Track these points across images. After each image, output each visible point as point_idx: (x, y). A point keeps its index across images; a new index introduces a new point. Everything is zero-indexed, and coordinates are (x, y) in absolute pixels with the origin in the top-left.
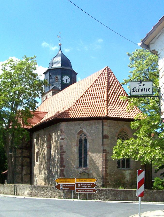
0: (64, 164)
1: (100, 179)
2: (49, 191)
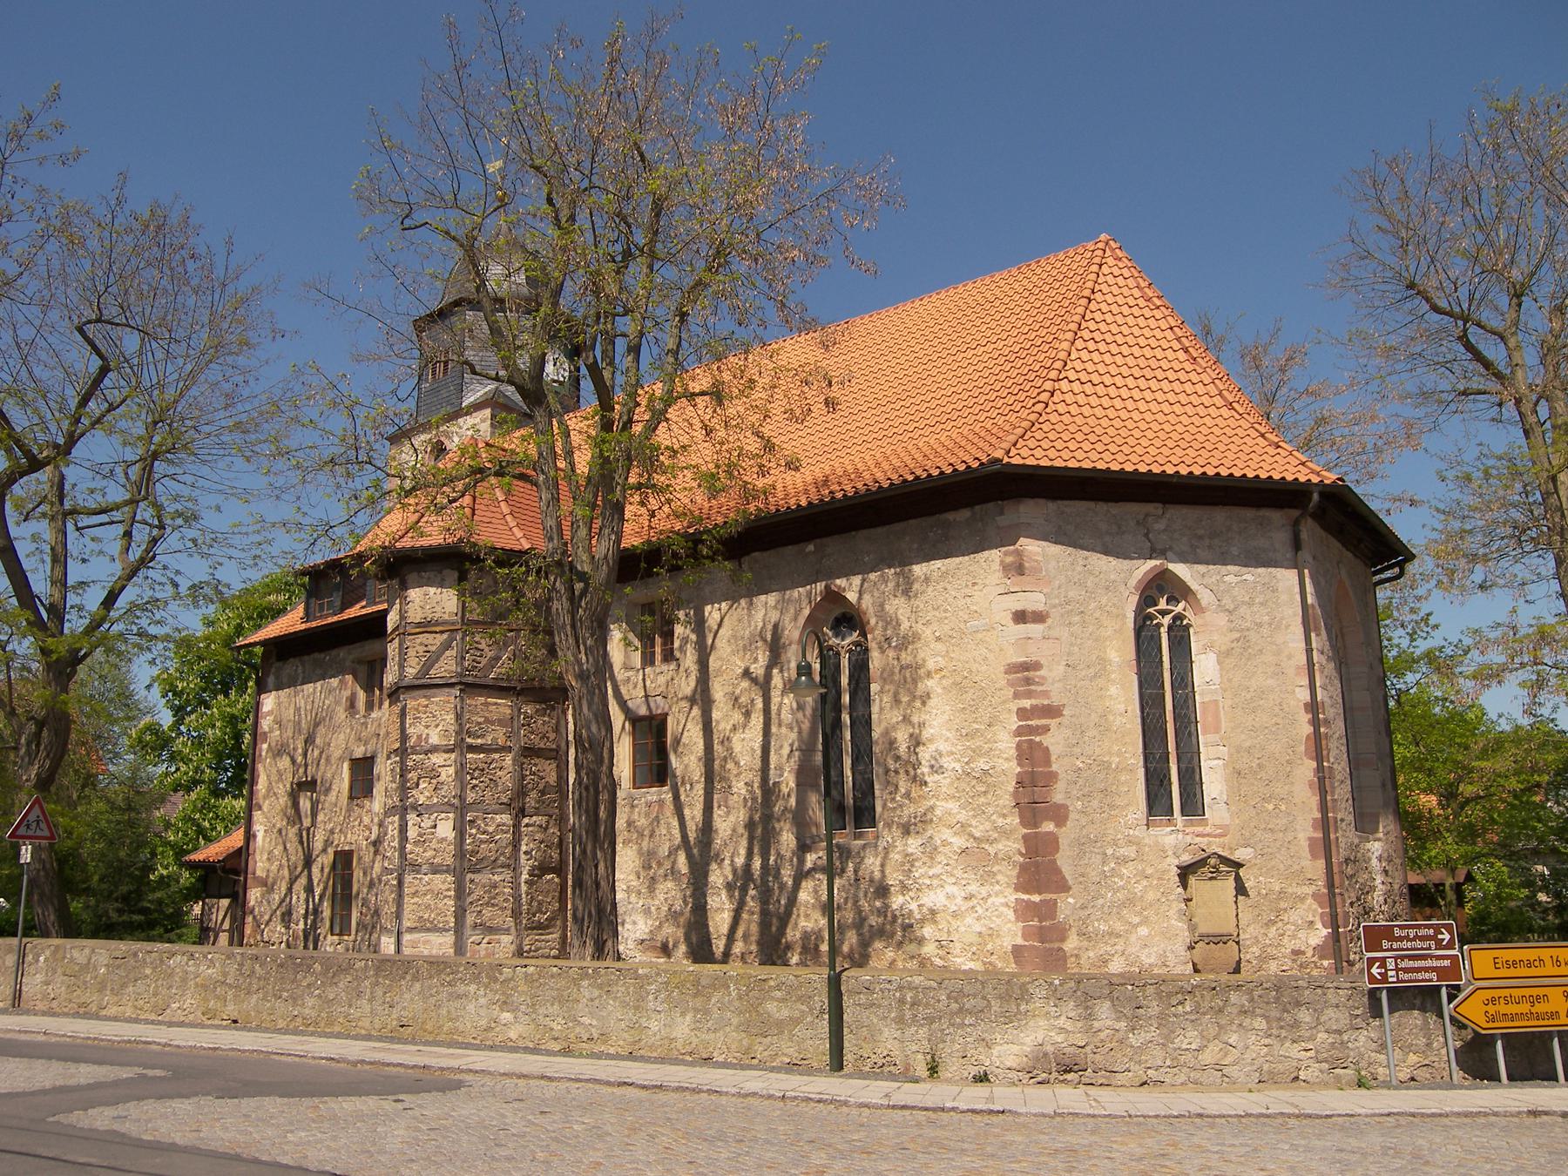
0: (1058, 797)
1: (1310, 901)
2: (1247, 1022)
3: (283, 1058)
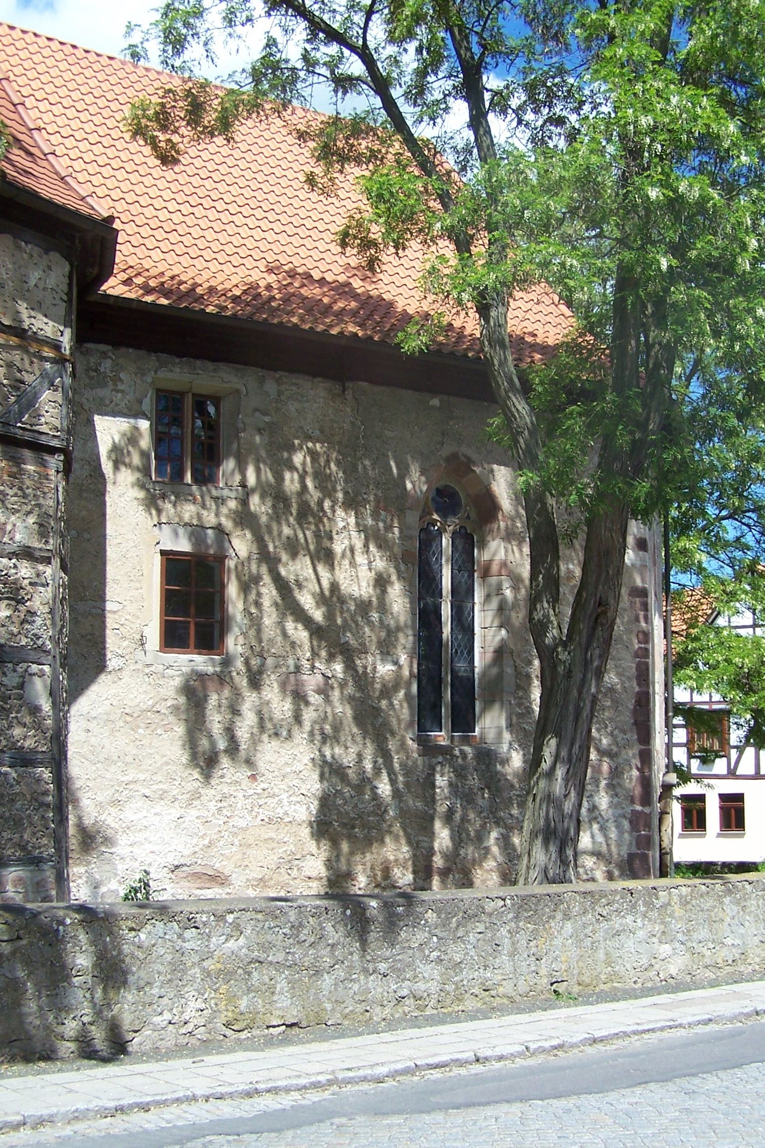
3: (138, 1121)
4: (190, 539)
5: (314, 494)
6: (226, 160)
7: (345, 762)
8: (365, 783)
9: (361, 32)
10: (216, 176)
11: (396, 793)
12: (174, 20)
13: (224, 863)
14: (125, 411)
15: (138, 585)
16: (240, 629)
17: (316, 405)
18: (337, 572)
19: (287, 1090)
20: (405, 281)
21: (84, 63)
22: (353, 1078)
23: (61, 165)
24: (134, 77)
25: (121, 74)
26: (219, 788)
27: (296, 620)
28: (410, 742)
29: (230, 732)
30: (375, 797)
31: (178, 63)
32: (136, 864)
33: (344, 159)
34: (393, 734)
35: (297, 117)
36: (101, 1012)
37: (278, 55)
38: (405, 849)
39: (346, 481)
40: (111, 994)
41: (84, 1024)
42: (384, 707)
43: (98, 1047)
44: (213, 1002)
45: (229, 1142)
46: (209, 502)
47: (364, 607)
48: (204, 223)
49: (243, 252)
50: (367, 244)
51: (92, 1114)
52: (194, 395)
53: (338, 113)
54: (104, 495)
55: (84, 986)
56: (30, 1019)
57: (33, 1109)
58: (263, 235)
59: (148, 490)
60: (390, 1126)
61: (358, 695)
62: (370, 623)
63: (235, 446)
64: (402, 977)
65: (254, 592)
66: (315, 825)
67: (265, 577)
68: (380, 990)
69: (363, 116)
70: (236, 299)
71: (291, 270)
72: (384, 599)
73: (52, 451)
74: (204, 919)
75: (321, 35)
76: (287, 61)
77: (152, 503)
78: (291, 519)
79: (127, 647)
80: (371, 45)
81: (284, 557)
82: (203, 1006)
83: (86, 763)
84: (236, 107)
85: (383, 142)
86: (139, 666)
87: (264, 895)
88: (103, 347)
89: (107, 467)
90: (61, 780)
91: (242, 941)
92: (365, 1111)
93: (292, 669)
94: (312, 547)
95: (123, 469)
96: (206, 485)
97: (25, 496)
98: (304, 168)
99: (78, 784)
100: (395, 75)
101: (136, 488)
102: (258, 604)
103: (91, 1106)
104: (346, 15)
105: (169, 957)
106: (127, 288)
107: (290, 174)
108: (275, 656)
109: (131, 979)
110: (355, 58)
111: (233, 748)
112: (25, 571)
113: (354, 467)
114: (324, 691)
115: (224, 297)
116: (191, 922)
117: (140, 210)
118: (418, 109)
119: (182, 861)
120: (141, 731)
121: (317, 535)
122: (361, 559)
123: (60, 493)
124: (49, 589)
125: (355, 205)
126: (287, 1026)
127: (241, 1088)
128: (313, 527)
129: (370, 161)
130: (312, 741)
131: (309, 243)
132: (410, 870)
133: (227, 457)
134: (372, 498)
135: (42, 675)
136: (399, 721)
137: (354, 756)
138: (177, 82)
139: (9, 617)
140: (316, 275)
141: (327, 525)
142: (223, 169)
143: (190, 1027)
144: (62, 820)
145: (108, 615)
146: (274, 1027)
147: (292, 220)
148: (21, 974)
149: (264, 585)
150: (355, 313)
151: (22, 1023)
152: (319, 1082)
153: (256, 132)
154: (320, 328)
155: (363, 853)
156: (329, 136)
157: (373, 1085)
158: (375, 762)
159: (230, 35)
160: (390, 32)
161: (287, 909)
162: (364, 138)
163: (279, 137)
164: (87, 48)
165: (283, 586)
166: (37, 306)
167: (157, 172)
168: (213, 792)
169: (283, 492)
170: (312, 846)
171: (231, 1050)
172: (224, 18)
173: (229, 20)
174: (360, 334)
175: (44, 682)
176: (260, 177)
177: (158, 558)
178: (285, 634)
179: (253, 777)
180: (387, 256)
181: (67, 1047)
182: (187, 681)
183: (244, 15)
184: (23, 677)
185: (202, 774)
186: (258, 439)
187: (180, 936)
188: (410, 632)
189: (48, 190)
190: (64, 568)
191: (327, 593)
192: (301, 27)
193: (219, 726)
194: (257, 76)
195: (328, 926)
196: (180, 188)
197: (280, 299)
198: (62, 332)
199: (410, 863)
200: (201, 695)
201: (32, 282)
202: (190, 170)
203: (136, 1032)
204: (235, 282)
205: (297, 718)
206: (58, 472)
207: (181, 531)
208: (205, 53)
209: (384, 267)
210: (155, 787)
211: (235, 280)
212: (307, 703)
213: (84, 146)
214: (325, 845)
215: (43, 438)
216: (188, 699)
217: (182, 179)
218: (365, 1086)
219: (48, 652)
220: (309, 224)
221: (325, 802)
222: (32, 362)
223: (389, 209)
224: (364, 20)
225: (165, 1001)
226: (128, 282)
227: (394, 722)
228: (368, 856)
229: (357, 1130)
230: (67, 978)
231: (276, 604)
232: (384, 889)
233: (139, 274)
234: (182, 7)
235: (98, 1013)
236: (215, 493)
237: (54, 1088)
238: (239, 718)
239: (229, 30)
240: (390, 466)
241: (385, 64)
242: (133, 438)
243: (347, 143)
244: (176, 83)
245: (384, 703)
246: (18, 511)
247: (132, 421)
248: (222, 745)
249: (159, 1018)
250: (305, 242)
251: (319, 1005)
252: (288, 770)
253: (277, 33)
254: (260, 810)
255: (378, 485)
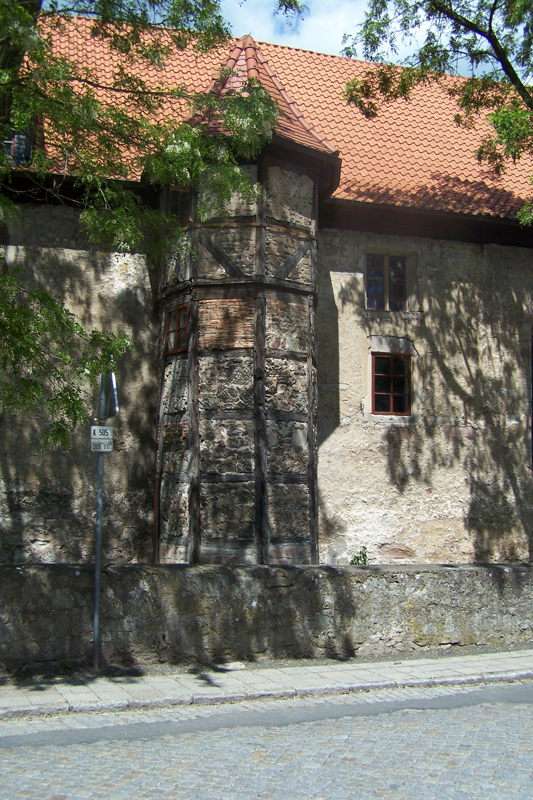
3: (362, 697)
4: (389, 345)
5: (465, 315)
6: (396, 110)
7: (486, 481)
8: (498, 494)
9: (487, 22)
10: (398, 122)
11: (518, 501)
12: (371, 29)
13: (412, 543)
14: (348, 268)
15: (358, 373)
16: (421, 399)
17: (465, 260)
18: (480, 363)
19: (453, 684)
20: (518, 179)
21: (317, 62)
22: (494, 678)
23: (306, 123)
24: (346, 67)
25: (339, 65)
26: (409, 497)
27: (455, 394)
28: (527, 469)
29: (415, 463)
30: (505, 503)
31: (374, 55)
32: (358, 543)
33: (478, 104)
34: (516, 464)
35: (448, 81)
36: (339, 631)
37: (436, 43)
38: (524, 536)
39: (485, 306)
40: (346, 621)
41: (329, 638)
42: (510, 447)
43: (338, 652)
44: (407, 627)
45: (418, 713)
46: (400, 322)
47: (497, 384)
48: (392, 151)
49: (416, 167)
50: (494, 157)
51: (335, 691)
52: (389, 257)
53: (474, 76)
54: (337, 319)
55: (330, 615)
56: (298, 633)
57: (301, 687)
58: (428, 156)
59: (363, 316)
60: (519, 710)
61: (494, 440)
62: (502, 395)
63: (415, 287)
64: (524, 617)
65: (429, 377)
66: (467, 521)
67: (436, 367)
68: (510, 624)
69: (489, 75)
70: (413, 197)
71: (447, 176)
72: (510, 380)
73: (306, 294)
74: (402, 577)
75: (462, 27)
76: (441, 46)
77: (365, 323)
78: (451, 331)
79: (353, 411)
80: (495, 29)
81: (447, 355)
82: (401, 630)
83: (328, 481)
84: (410, 78)
85: (502, 90)
86: (360, 423)
87: (436, 563)
88: (334, 230)
89: (338, 302)
90: (314, 491)
91: (425, 591)
92: (502, 700)
93: (453, 424)
94: (464, 348)
95: (348, 303)
96: (398, 311)
97: (291, 321)
98: (452, 112)
99: (324, 494)
100: (509, 47)
101: (356, 315)
102: (431, 384)
103: (334, 687)
104: (478, 13)
105: (380, 600)
106: (347, 194)
107: (444, 117)
108: (442, 416)
109: (357, 612)
110: (484, 39)
111: (417, 473)
112: (292, 366)
113: (490, 298)
114: (473, 437)
115: (406, 196)
116: (393, 579)
117: (353, 146)
118: (524, 68)
119: (386, 542)
120: (361, 462)
121: (468, 341)
122: (495, 355)
123: (311, 319)
124: (306, 377)
125: (486, 133)
126: (452, 644)
127: (425, 681)
128: (465, 336)
129: (494, 105)
130: (466, 468)
131: (457, 159)
132: (527, 549)
133: (411, 295)
134: (501, 316)
135: (302, 428)
136: (520, 456)
137: (492, 478)
138: (372, 67)
139: (283, 394)
140: (462, 179)
141: (474, 334)
142: (402, 117)
143: (393, 642)
144: (315, 515)
145: (341, 392)
146: (444, 644)
147: (446, 145)
148: (293, 606)
149: (435, 372)
150: (487, 201)
151: (293, 636)
152: (473, 680)
153: (421, 93)
154: (466, 211)
155: (498, 539)
156: (468, 91)
157: (507, 684)
158: (505, 482)
159: (406, 34)
160: (506, 20)
161: (453, 572)
162: (490, 90)
163: (436, 95)
164: (333, 55)
165: (446, 372)
166: (295, 208)
167: (362, 123)
168: (405, 499)
169: (446, 314)
170: (465, 534)
171: (417, 658)
172: (401, 24)
173: (404, 25)
174: (492, 214)
175: (304, 433)
176: (425, 120)
177: (370, 357)
178: (448, 402)
179: (429, 491)
180: (508, 163)
181: (319, 651)
182: (389, 431)
183: (414, 21)
184: (291, 430)
185: (398, 488)
186: (429, 282)
187: (387, 587)
188: (527, 400)
189: (299, 138)
190: (314, 364)
191: (474, 376)
192: (449, 24)
193: (408, 459)
194: (422, 57)
195: (478, 583)
196: (377, 131)
197: (441, 195)
198: (310, 223)
199: (527, 545)
200: (397, 440)
201: (292, 194)
202: (382, 119)
203: (360, 644)
204: (412, 186)
205: (457, 454)
206: (310, 306)
207: (384, 340)
208: (391, 47)
209: (506, 171)
210: (369, 496)
211: (412, 185)
212: (463, 445)
213: (319, 110)
214: (474, 533)
215: (301, 286)
216: (390, 442)
217: (378, 125)
218: (501, 684)
219: (306, 415)
220: (457, 147)
221: (474, 506)
222: (293, 241)
223: (509, 134)
224: (489, 14)
225: (378, 626)
226: (348, 190)
227: (517, 457)
228: (501, 540)
229: (498, 711)
230: (320, 610)
231: (442, 384)
232: (511, 561)
233: (354, 185)
234: (376, 21)
235: (338, 632)
236: (403, 316)
237: (313, 675)
238: (421, 454)
239: (405, 31)
240: (513, 297)
241: (503, 41)
242: (353, 284)
243: (479, 94)
244: (372, 67)
245: (510, 445)
246: (287, 331)
247: (352, 274)
248: (410, 471)
249: (374, 636)
250: (454, 158)
251: (472, 632)
252: (451, 486)
253: (434, 30)
254: (434, 511)
255: (505, 308)
